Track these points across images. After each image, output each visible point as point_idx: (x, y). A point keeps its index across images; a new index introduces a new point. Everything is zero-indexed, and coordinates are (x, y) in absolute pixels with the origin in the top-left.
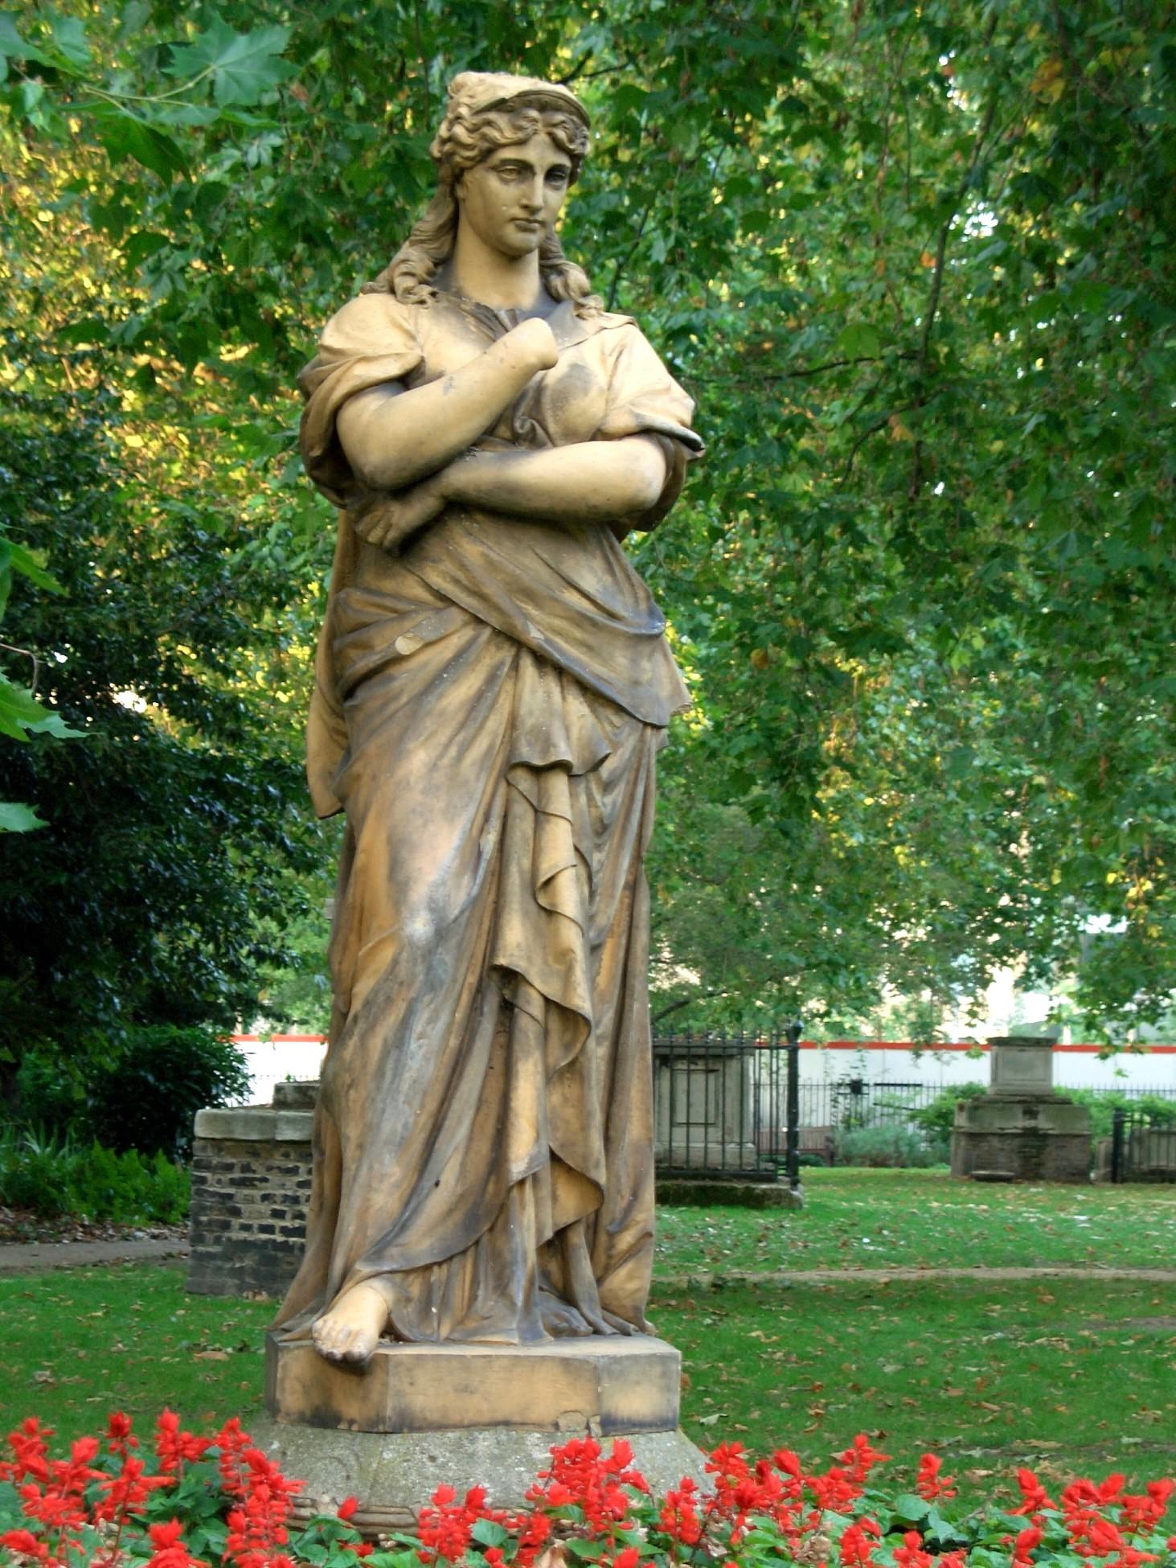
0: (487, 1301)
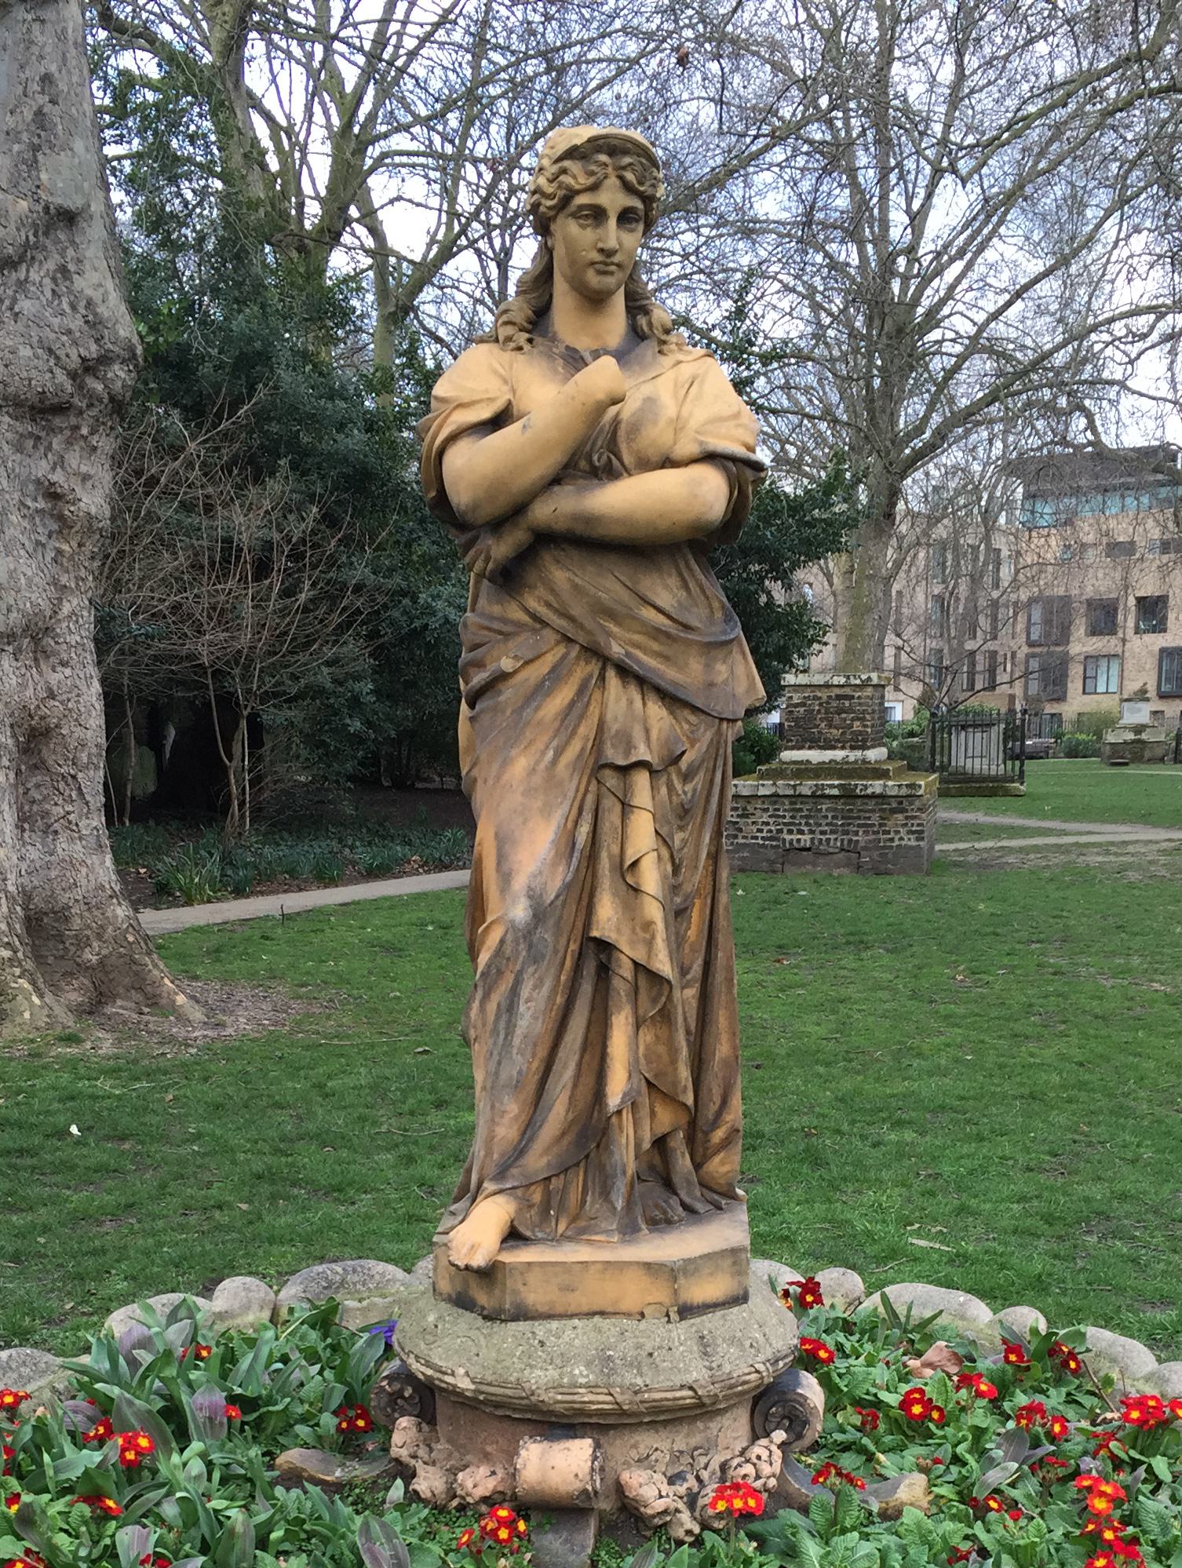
0: (593, 1205)
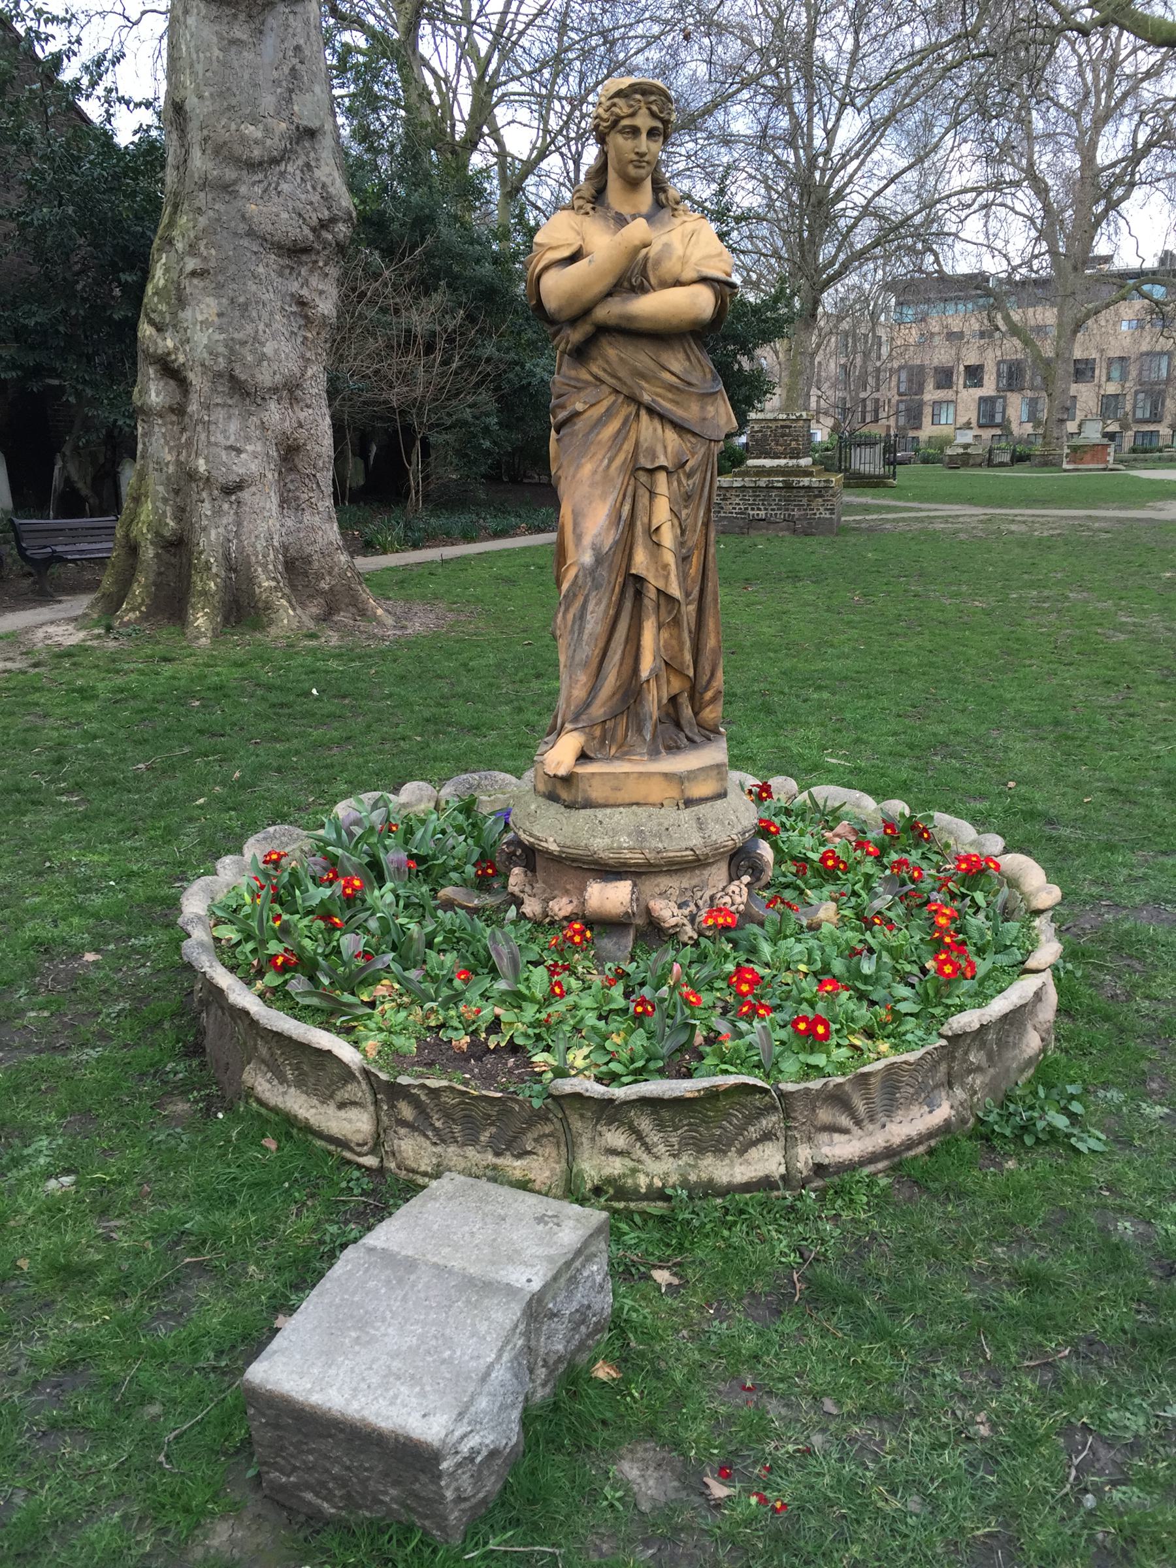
0: (632, 738)
